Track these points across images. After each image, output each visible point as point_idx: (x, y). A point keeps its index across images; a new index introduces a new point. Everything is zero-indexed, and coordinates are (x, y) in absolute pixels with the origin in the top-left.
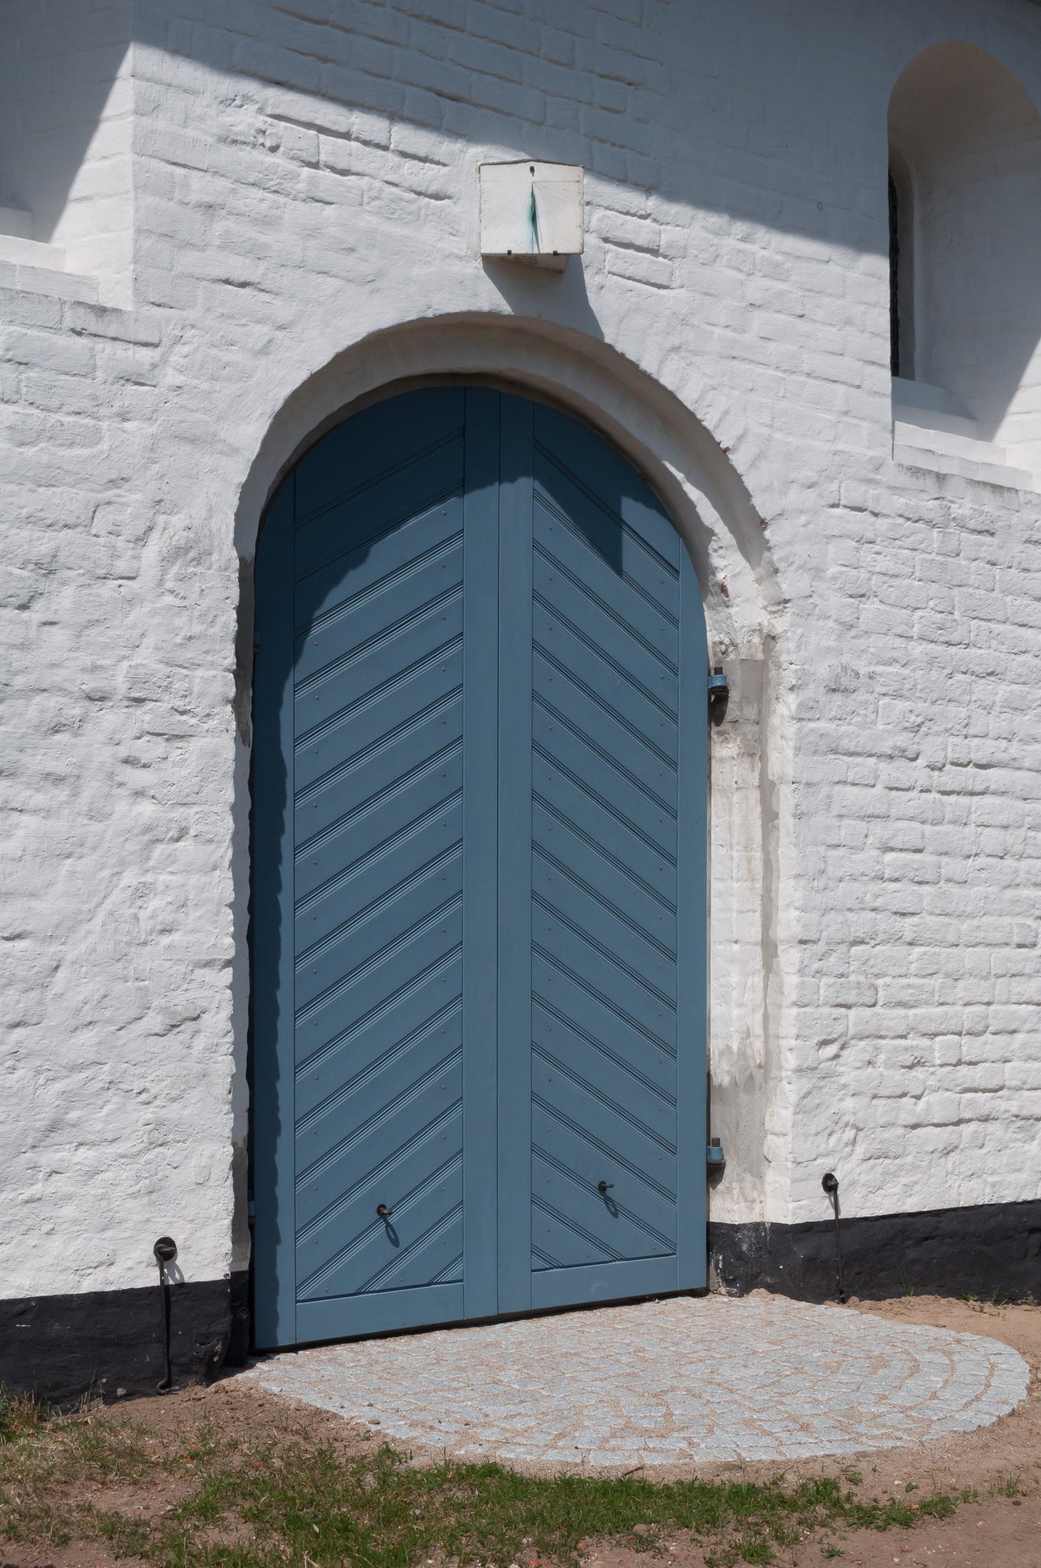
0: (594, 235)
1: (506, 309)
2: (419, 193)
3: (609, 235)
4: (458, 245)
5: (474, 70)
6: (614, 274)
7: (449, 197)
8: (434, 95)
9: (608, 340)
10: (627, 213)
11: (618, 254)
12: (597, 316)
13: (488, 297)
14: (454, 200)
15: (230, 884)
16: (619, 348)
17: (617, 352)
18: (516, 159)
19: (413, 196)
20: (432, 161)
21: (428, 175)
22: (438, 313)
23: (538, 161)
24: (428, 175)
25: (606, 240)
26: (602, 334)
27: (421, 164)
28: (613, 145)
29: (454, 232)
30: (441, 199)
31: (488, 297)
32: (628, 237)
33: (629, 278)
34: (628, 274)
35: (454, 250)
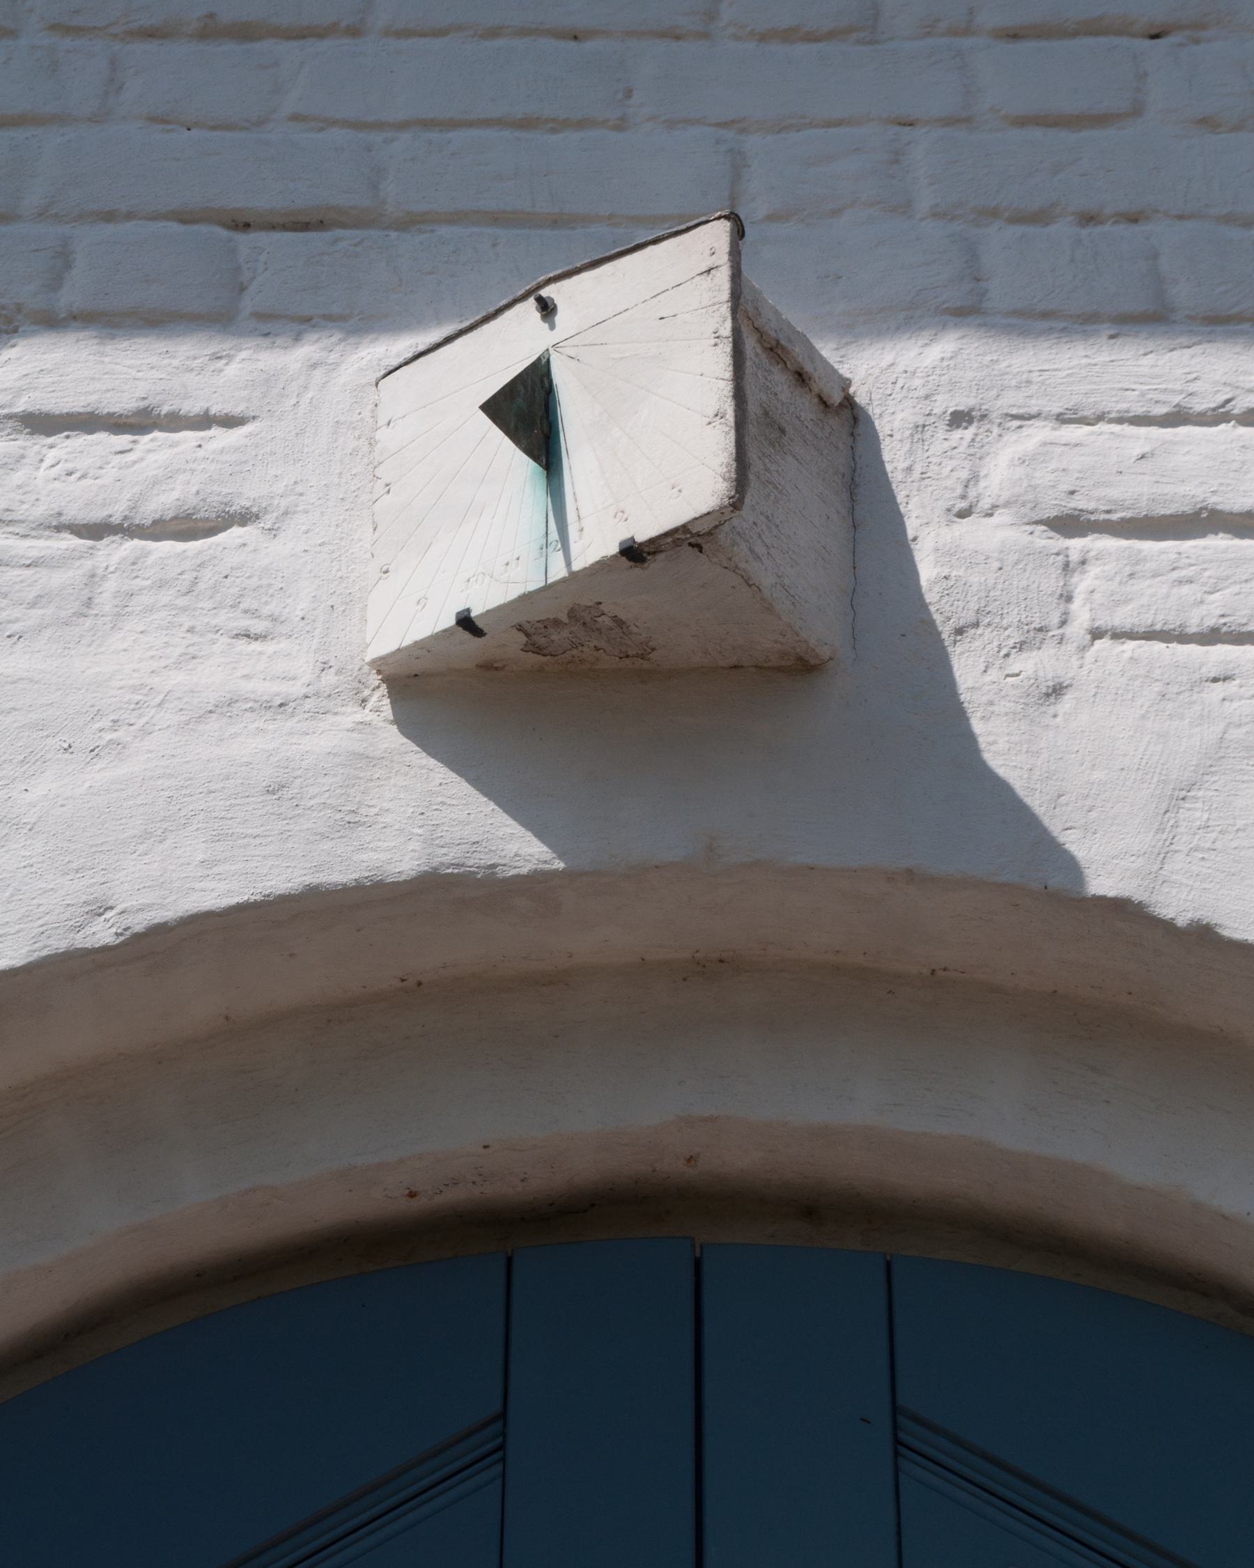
0: (1002, 517)
1: (518, 848)
2: (96, 531)
3: (1079, 503)
4: (288, 665)
5: (403, 126)
6: (1120, 635)
7: (245, 518)
8: (175, 227)
9: (1103, 882)
10: (1178, 418)
11: (1139, 560)
12: (1037, 803)
13: (431, 817)
14: (268, 521)
15: (886, 456)
16: (1177, 903)
17: (1167, 926)
18: (466, 324)
19: (70, 542)
20: (175, 422)
21: (161, 470)
22: (139, 923)
23: (549, 281)
24: (161, 470)
25: (1069, 524)
26: (1072, 867)
27: (124, 440)
28: (1088, 219)
29: (258, 626)
30: (211, 530)
31: (431, 817)
32: (1183, 494)
33: (1211, 637)
34: (1196, 620)
35: (247, 687)
